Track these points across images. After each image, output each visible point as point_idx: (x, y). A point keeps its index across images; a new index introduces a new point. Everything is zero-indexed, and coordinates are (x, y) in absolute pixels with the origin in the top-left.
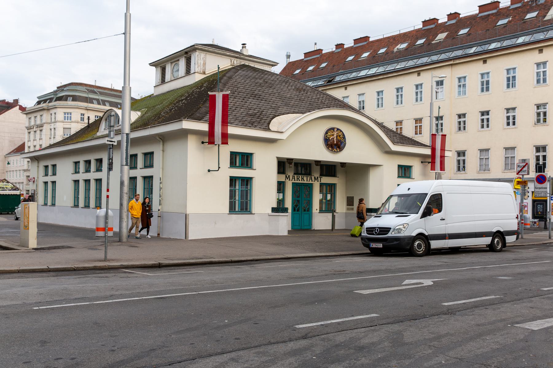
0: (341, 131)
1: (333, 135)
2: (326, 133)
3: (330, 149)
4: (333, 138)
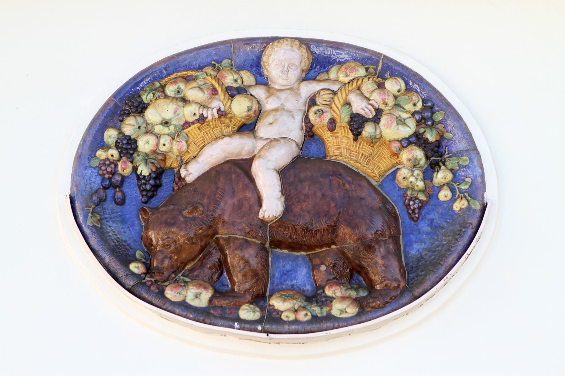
0: (382, 68)
1: (247, 127)
2: (129, 102)
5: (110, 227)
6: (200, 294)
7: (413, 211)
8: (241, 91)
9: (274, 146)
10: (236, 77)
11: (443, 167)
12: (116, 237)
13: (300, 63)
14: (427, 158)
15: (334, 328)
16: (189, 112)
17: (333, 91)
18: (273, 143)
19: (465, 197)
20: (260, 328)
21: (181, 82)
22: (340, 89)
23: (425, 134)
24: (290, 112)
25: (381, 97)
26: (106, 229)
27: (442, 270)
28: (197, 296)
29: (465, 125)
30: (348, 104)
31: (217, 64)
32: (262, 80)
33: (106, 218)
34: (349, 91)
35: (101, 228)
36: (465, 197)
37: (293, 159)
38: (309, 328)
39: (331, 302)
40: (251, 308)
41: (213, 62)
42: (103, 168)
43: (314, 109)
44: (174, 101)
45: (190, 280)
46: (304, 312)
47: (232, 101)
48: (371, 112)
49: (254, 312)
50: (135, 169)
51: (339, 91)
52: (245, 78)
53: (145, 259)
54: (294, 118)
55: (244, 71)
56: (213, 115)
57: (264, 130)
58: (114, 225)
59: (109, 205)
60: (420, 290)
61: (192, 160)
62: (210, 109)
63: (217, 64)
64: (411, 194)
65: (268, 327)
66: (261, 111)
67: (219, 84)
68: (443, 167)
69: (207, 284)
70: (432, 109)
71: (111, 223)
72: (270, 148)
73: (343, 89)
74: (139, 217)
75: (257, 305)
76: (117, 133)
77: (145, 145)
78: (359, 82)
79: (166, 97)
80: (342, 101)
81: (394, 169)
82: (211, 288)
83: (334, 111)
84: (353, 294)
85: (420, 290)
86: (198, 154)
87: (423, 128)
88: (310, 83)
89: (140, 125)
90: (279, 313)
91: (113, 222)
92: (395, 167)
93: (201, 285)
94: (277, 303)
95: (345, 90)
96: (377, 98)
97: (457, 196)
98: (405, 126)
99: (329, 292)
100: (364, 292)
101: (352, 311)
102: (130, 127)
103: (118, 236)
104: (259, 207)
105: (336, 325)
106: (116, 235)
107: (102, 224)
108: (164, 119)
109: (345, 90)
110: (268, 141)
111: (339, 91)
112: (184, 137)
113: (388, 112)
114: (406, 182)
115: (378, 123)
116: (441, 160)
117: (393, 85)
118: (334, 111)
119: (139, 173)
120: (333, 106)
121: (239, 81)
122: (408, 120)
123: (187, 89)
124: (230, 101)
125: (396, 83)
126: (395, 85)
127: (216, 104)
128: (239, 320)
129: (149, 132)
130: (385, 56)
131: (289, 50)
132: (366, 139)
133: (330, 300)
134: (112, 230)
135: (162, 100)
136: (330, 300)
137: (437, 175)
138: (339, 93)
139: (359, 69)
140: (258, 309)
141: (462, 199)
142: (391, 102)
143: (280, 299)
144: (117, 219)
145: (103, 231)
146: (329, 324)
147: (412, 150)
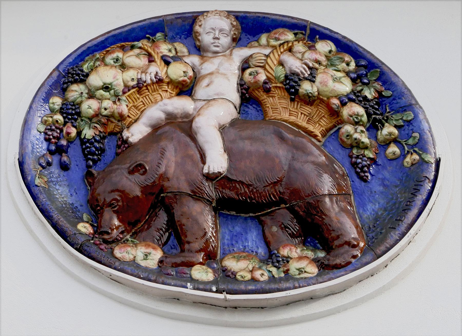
2: (71, 73)
3: (148, 255)
4: (183, 125)
5: (57, 190)
6: (150, 254)
7: (362, 169)
8: (177, 58)
9: (212, 105)
10: (170, 47)
11: (386, 124)
12: (63, 200)
13: (230, 31)
14: (369, 115)
15: (295, 288)
16: (131, 76)
17: (265, 55)
18: (211, 103)
19: (415, 151)
20: (214, 289)
21: (118, 51)
22: (272, 52)
23: (363, 92)
24: (225, 75)
25: (318, 40)
26: (53, 191)
27: (403, 227)
28: (146, 256)
29: (402, 81)
30: (281, 64)
31: (151, 37)
32: (199, 50)
33: (52, 182)
34: (281, 53)
35: (49, 190)
36: (415, 151)
37: (232, 120)
38: (267, 287)
39: (288, 262)
40: (203, 268)
41: (147, 36)
42: (50, 133)
43: (248, 71)
44: (114, 68)
45: (138, 242)
46: (260, 272)
47: (167, 68)
48: (306, 71)
49: (207, 272)
50: (79, 133)
51: (272, 53)
52: (178, 49)
53: (92, 221)
54: (229, 80)
55: (177, 43)
56: (151, 79)
57: (201, 91)
58: (61, 188)
59: (55, 170)
60: (383, 248)
61: (133, 123)
62: (147, 74)
63: (151, 37)
64: (357, 153)
65: (222, 287)
66: (196, 78)
67: (154, 52)
68: (386, 124)
69: (156, 246)
70: (367, 68)
71: (57, 187)
72: (208, 107)
73: (275, 51)
74: (85, 181)
75: (209, 266)
76: (61, 101)
77: (89, 107)
78: (290, 44)
79: (106, 65)
80: (276, 62)
81: (336, 129)
82: (160, 249)
83: (268, 72)
84: (310, 254)
85: (383, 248)
86: (138, 119)
87: (360, 86)
88: (241, 49)
89: (82, 91)
90: (234, 274)
91: (60, 186)
92: (336, 126)
93: (149, 246)
94: (231, 264)
95: (277, 52)
96: (310, 56)
97: (406, 152)
98: (341, 84)
99: (285, 252)
100: (321, 253)
101: (313, 270)
102: (76, 91)
103: (65, 199)
104: (202, 165)
105: (297, 285)
106: (63, 198)
107: (49, 186)
108: (105, 84)
109: (277, 52)
110: (206, 102)
111: (272, 53)
112: (125, 101)
113: (322, 71)
114: (349, 140)
115: (314, 82)
116: (383, 119)
117: (324, 47)
118: (268, 72)
119: (82, 137)
120: (267, 67)
121: (174, 52)
122: (343, 78)
123: (125, 57)
124: (166, 69)
125: (327, 45)
126: (326, 46)
127: (153, 69)
128: (192, 280)
129: (91, 96)
130: (311, 22)
131: (218, 19)
132: (303, 98)
133: (287, 259)
134: (59, 193)
135: (102, 68)
136: (287, 259)
137: (381, 133)
138: (271, 55)
139: (288, 34)
140: (210, 270)
141: (412, 154)
142: (323, 59)
143: (233, 259)
144: (63, 183)
145: (50, 193)
146: (288, 285)
147: (351, 107)
